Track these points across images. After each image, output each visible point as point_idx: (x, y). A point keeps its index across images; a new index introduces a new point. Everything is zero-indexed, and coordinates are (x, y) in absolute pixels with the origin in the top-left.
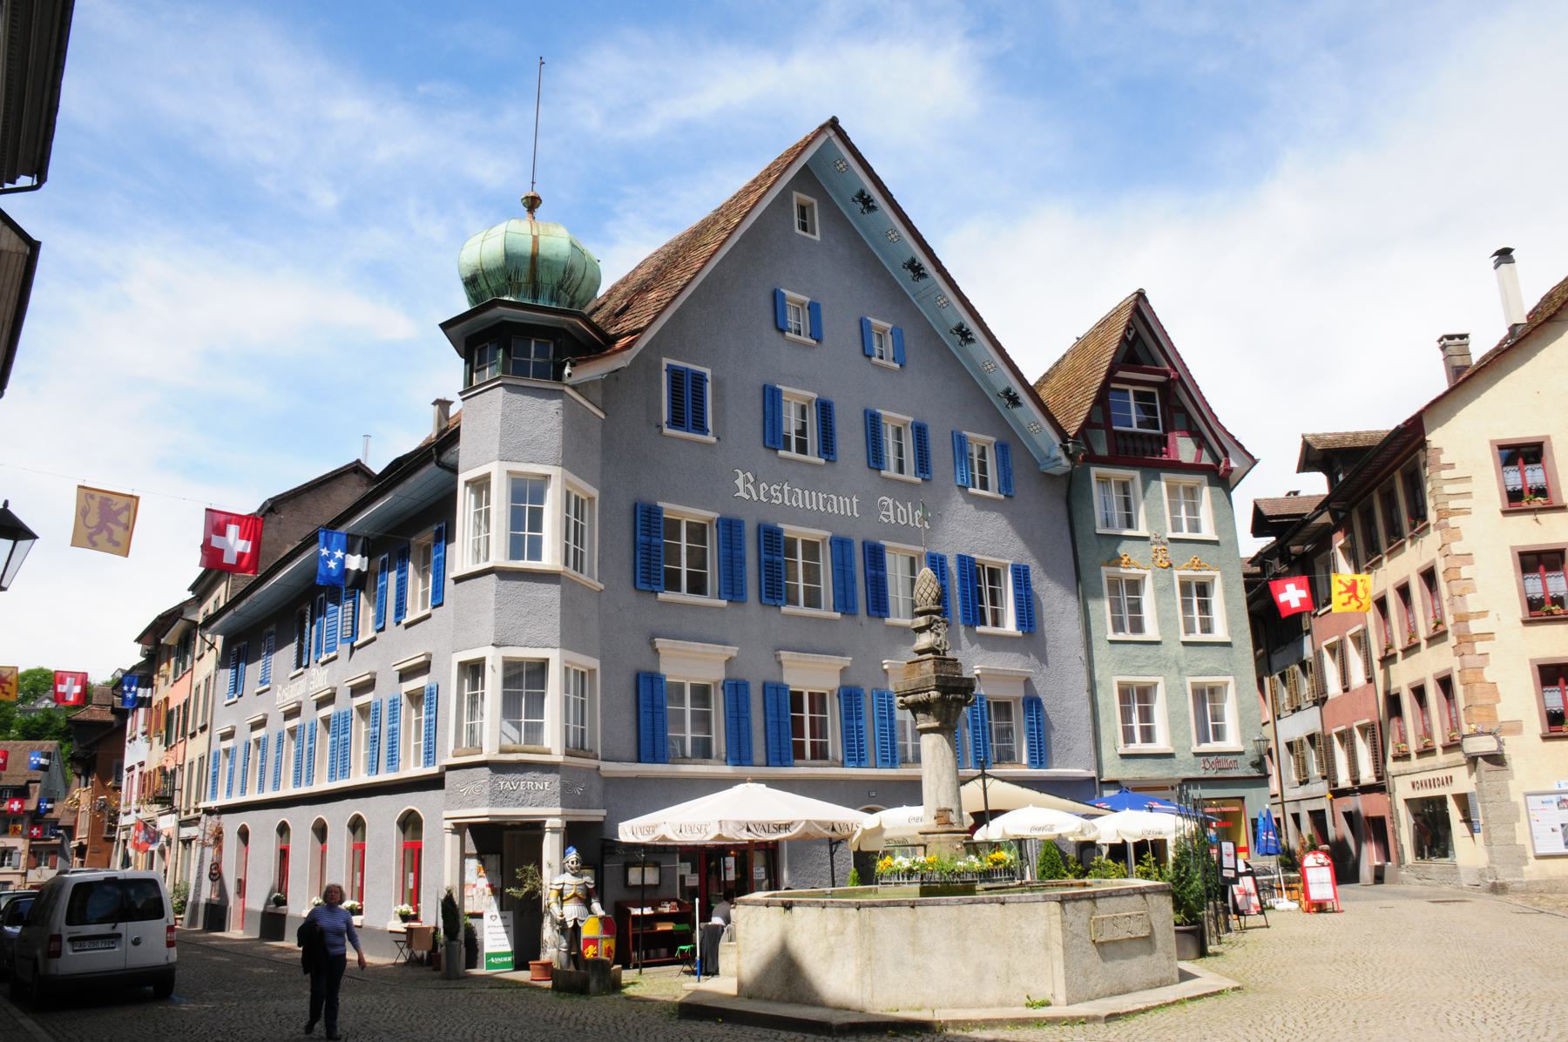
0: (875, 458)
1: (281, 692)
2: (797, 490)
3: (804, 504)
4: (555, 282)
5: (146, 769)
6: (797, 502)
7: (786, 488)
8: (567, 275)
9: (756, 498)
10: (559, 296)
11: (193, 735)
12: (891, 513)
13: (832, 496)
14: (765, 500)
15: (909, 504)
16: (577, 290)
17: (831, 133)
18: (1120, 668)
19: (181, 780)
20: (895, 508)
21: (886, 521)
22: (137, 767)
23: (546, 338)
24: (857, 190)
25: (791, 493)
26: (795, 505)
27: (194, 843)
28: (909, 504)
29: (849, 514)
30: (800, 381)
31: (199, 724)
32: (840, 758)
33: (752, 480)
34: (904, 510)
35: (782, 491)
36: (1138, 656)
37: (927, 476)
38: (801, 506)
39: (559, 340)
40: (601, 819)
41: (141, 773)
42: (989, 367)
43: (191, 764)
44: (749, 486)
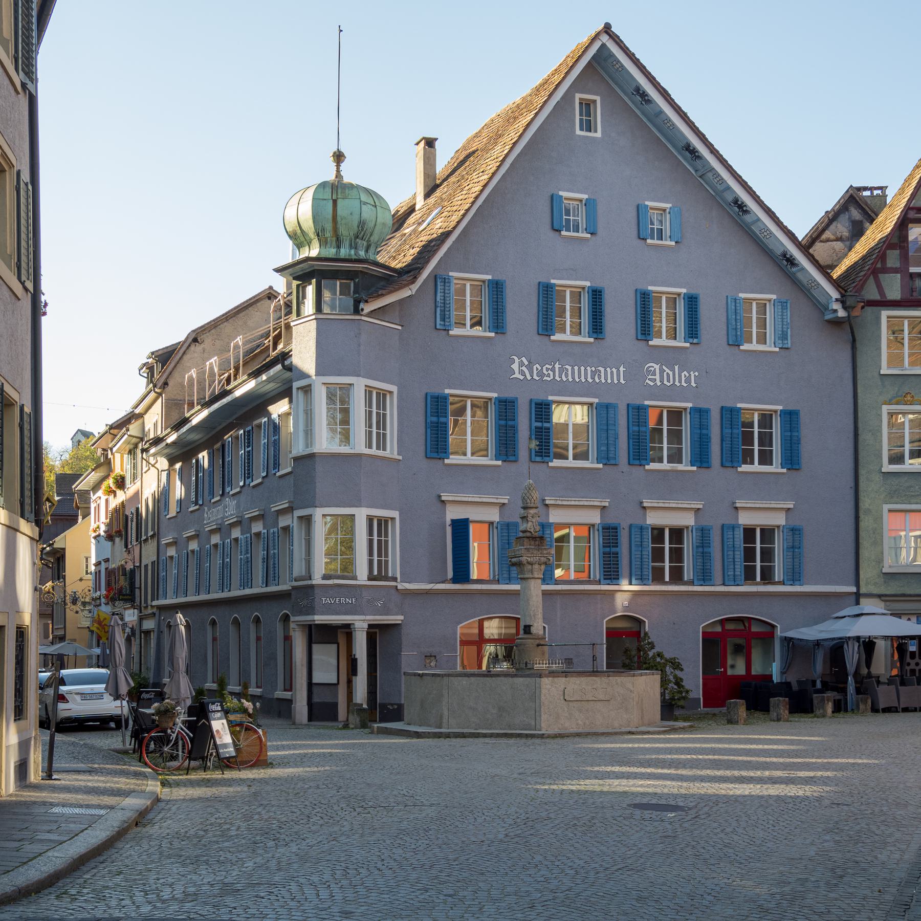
0: (645, 329)
1: (207, 513)
2: (567, 367)
3: (573, 378)
4: (352, 234)
5: (112, 566)
6: (567, 376)
7: (557, 366)
8: (360, 228)
9: (529, 378)
10: (356, 244)
11: (146, 540)
12: (657, 377)
13: (600, 368)
14: (537, 378)
15: (676, 367)
16: (371, 236)
17: (605, 38)
18: (892, 497)
19: (139, 580)
20: (662, 371)
21: (652, 384)
22: (103, 563)
23: (347, 279)
24: (634, 86)
25: (561, 370)
26: (565, 379)
27: (152, 633)
28: (676, 367)
29: (616, 382)
30: (573, 273)
31: (151, 533)
32: (598, 577)
33: (526, 363)
34: (671, 373)
35: (553, 370)
36: (911, 487)
37: (695, 341)
38: (571, 380)
39: (357, 280)
40: (400, 622)
41: (106, 569)
42: (765, 234)
43: (146, 566)
44: (524, 368)
